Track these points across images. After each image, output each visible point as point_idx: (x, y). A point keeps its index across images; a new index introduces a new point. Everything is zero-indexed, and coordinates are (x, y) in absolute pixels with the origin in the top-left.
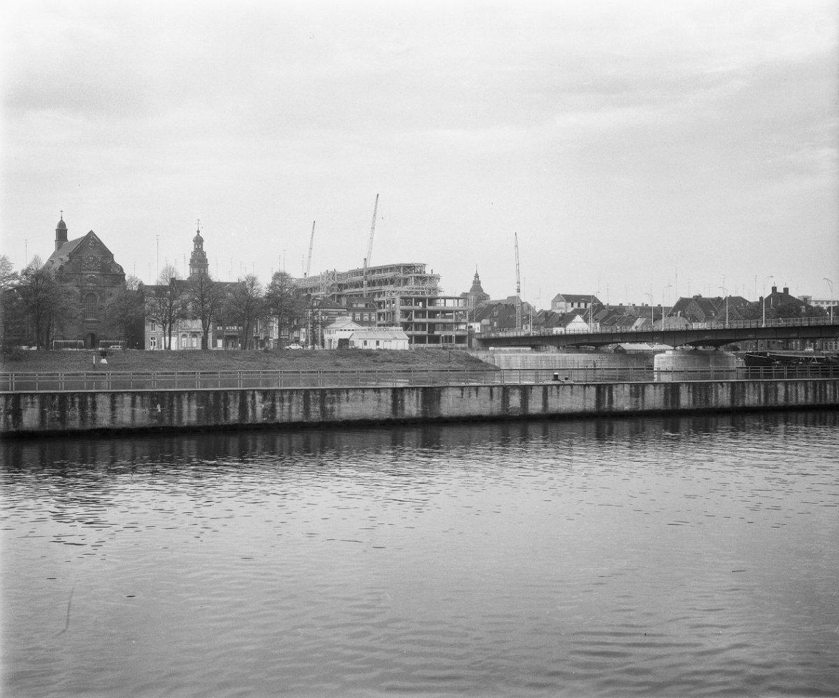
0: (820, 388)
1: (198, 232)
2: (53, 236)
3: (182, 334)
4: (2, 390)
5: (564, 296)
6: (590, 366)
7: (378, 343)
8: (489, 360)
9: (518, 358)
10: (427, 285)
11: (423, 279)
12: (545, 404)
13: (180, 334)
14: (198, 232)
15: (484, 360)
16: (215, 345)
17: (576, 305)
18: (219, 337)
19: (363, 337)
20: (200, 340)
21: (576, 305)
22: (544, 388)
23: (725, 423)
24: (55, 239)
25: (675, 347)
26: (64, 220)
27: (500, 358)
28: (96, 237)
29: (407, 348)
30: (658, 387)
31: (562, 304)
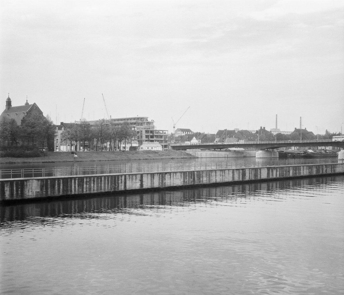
0: (98, 181)
1: (27, 101)
2: (5, 104)
3: (68, 144)
4: (3, 177)
5: (180, 129)
6: (226, 156)
7: (152, 148)
8: (194, 154)
9: (205, 154)
10: (151, 126)
11: (149, 123)
12: (125, 186)
13: (67, 145)
14: (27, 101)
15: (192, 154)
16: (80, 149)
17: (187, 132)
18: (81, 146)
19: (147, 146)
20: (74, 147)
21: (187, 132)
22: (11, 184)
23: (306, 181)
24: (6, 105)
25: (215, 149)
26: (10, 97)
27: (198, 153)
28: (37, 106)
29: (161, 150)
30: (158, 175)
31: (180, 132)
